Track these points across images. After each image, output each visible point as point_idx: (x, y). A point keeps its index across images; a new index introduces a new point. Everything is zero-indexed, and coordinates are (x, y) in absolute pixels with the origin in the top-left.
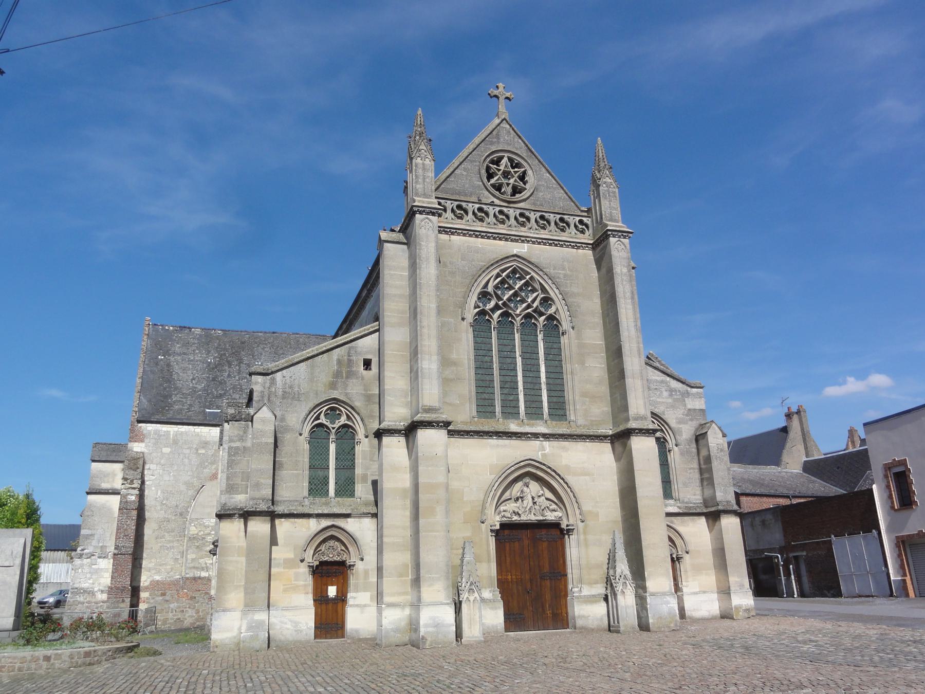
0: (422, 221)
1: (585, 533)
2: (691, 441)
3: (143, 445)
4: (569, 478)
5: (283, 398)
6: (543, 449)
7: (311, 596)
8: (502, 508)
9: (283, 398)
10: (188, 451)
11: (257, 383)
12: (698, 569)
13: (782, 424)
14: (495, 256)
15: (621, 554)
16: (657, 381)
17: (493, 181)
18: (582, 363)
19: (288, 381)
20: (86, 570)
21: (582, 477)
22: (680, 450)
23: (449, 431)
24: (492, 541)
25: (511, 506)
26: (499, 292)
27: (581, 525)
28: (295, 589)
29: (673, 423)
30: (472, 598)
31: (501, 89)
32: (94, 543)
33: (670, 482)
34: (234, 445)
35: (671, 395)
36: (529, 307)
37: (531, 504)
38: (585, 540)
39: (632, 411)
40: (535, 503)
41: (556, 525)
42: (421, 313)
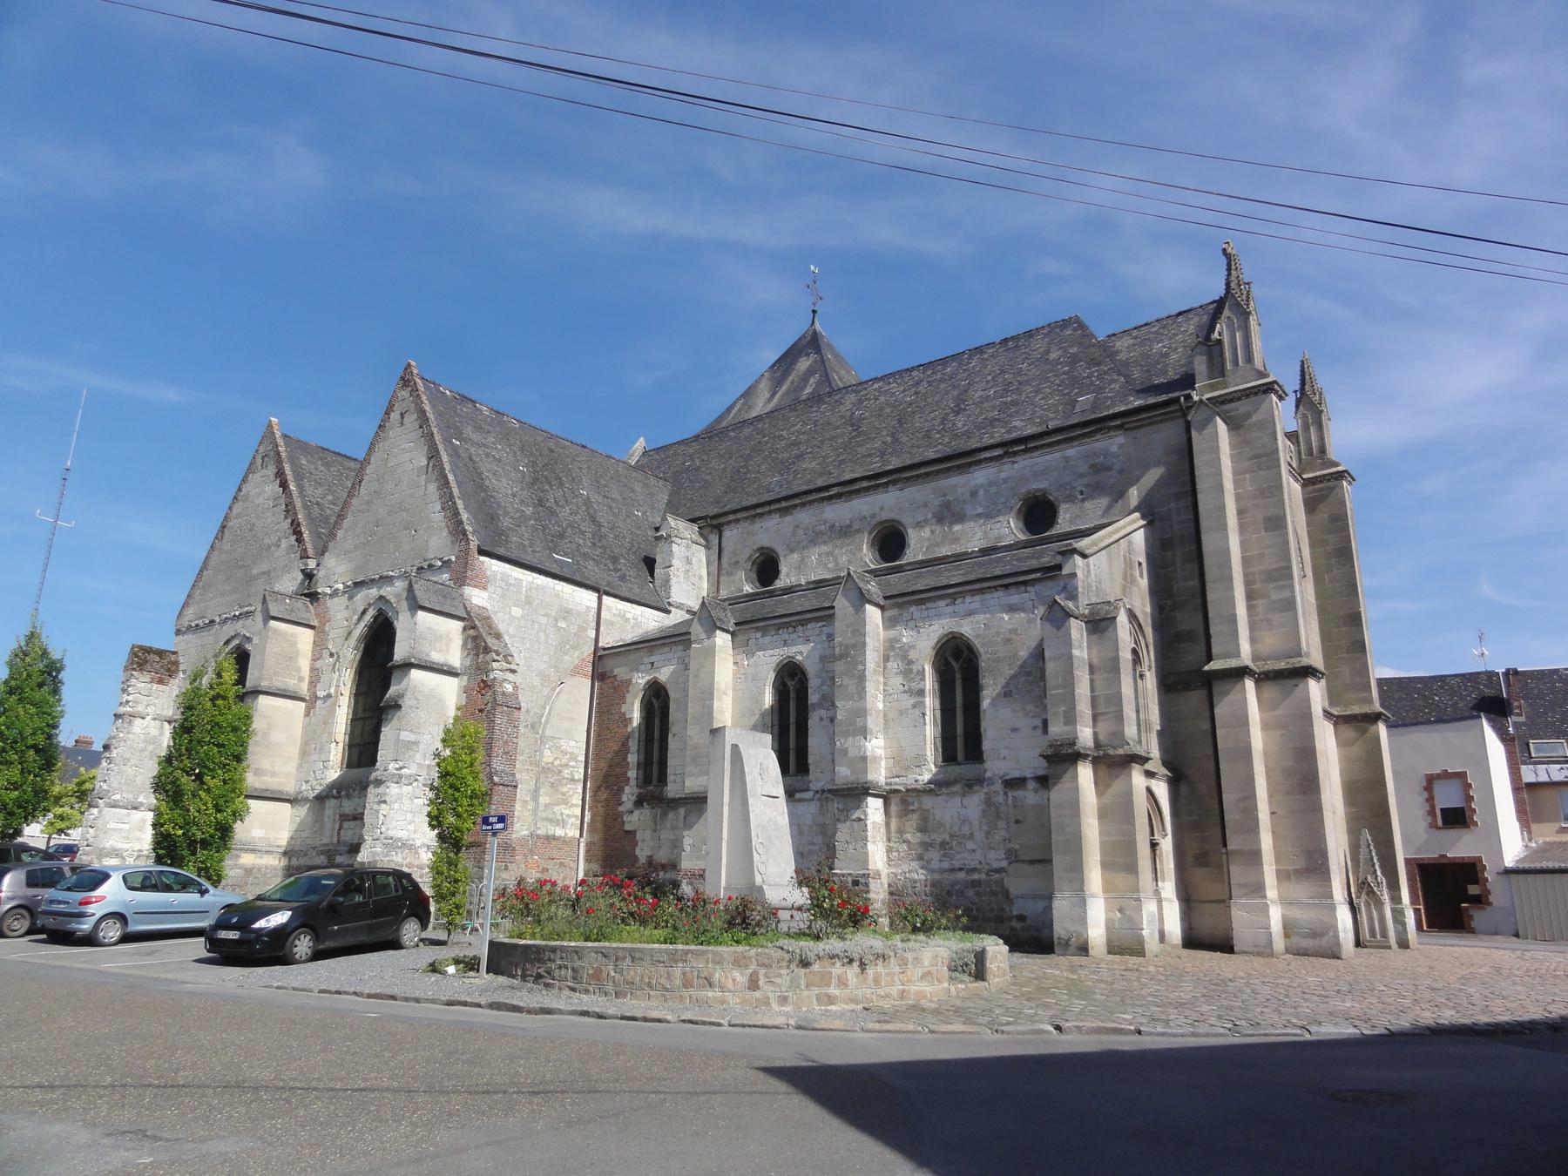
3: (484, 594)
10: (544, 620)
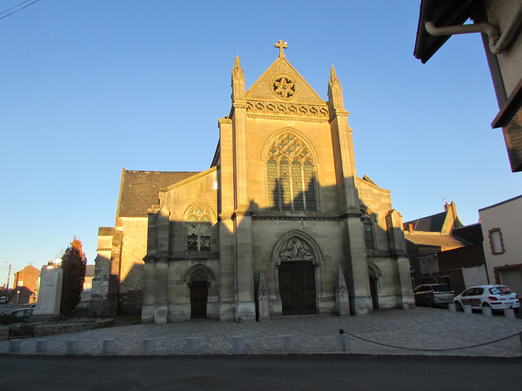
2: (383, 220)
4: (316, 239)
5: (174, 203)
6: (303, 224)
7: (189, 298)
9: (174, 203)
10: (143, 230)
11: (161, 196)
13: (443, 210)
15: (341, 276)
16: (365, 190)
17: (277, 90)
19: (176, 195)
20: (98, 286)
24: (277, 271)
26: (281, 147)
31: (281, 43)
32: (101, 273)
37: (297, 252)
39: (349, 204)
40: (299, 252)
41: (310, 262)
42: (238, 158)
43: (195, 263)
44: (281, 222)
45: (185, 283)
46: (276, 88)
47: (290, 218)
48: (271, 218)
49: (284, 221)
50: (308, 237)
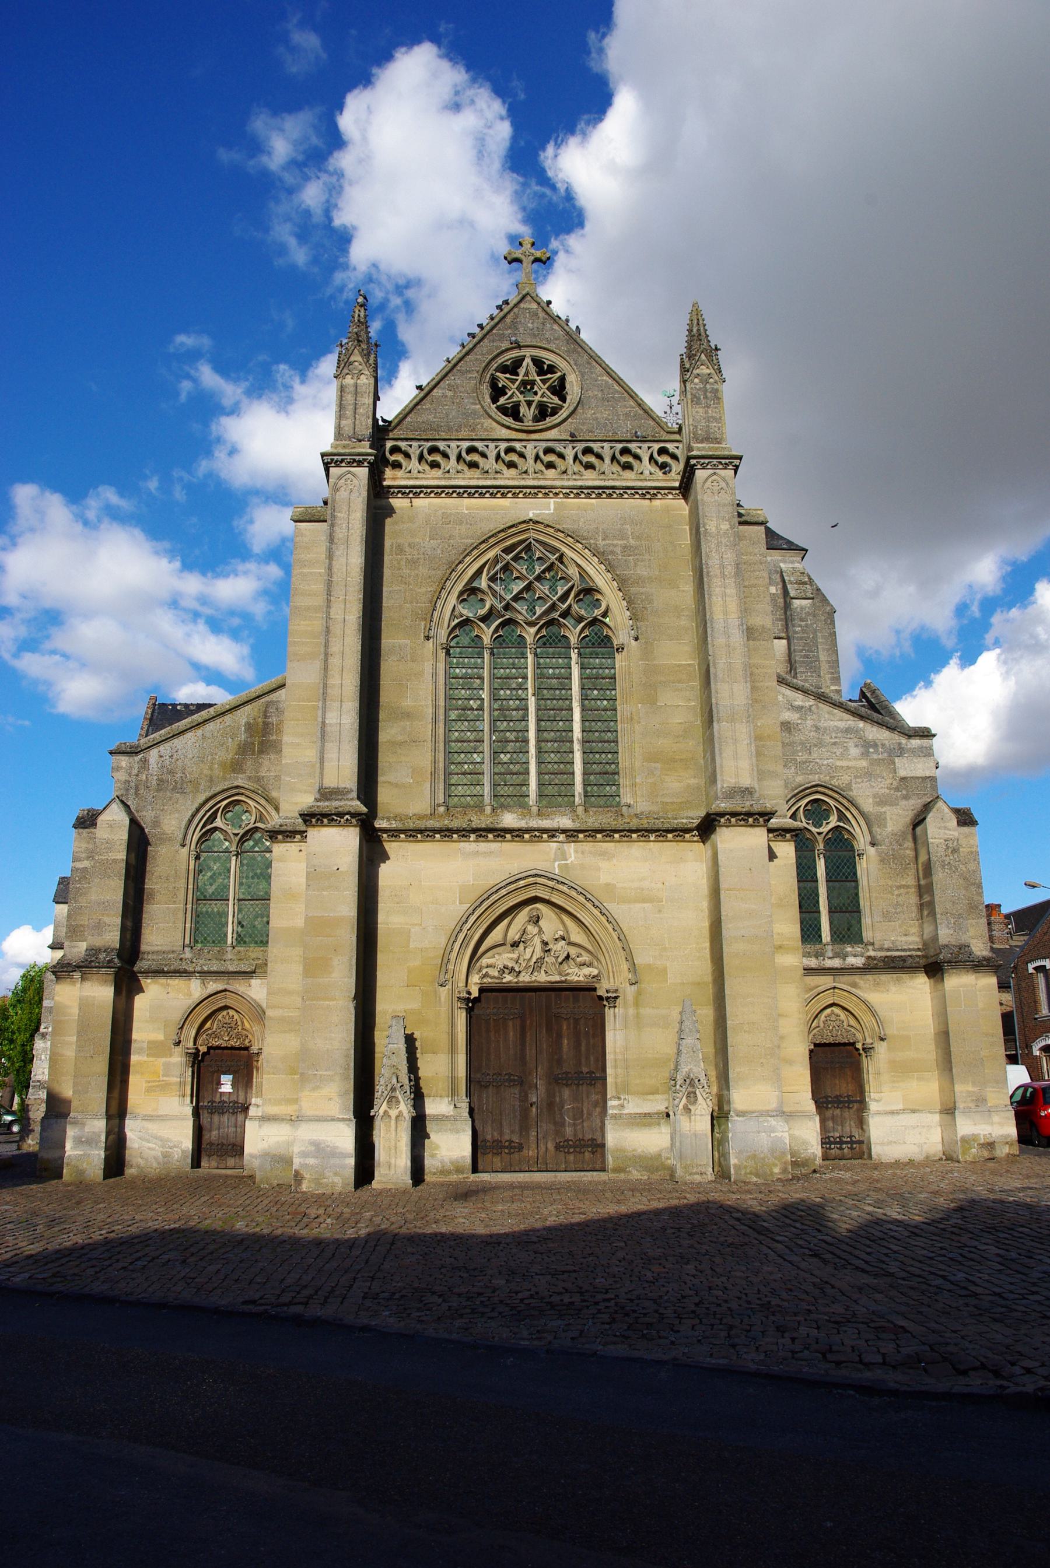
0: (340, 478)
1: (637, 1004)
4: (612, 907)
8: (484, 961)
9: (158, 790)
12: (903, 1070)
14: (492, 527)
16: (837, 729)
18: (651, 701)
21: (638, 905)
22: (879, 854)
23: (770, 831)
24: (461, 1018)
25: (505, 958)
27: (630, 991)
28: (163, 1087)
29: (868, 805)
30: (393, 1113)
33: (859, 912)
34: (79, 865)
35: (865, 754)
36: (553, 607)
37: (538, 953)
38: (638, 1016)
43: (213, 986)
44: (483, 846)
45: (178, 1049)
46: (497, 392)
47: (517, 834)
48: (447, 833)
49: (495, 846)
50: (581, 899)
